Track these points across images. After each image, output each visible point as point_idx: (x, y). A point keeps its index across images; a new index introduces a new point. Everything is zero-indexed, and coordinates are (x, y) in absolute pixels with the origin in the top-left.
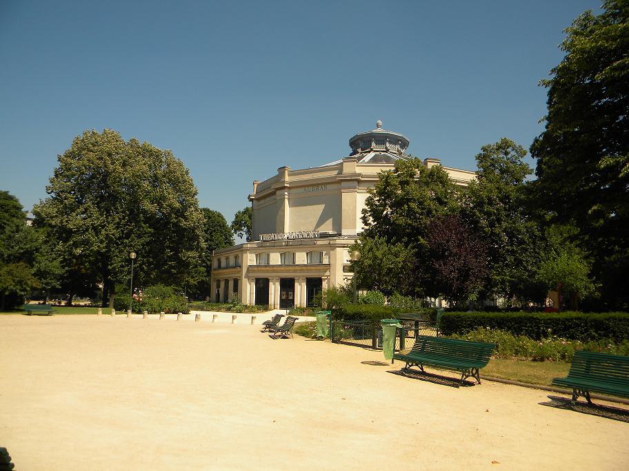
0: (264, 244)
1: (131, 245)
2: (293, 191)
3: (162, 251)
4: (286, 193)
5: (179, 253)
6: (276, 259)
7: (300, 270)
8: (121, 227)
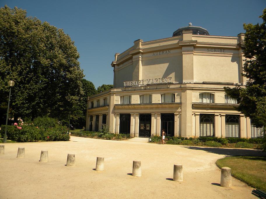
0: (127, 89)
1: (30, 89)
2: (145, 55)
3: (54, 94)
4: (140, 57)
5: (66, 96)
6: (136, 99)
7: (156, 108)
8: (23, 75)
